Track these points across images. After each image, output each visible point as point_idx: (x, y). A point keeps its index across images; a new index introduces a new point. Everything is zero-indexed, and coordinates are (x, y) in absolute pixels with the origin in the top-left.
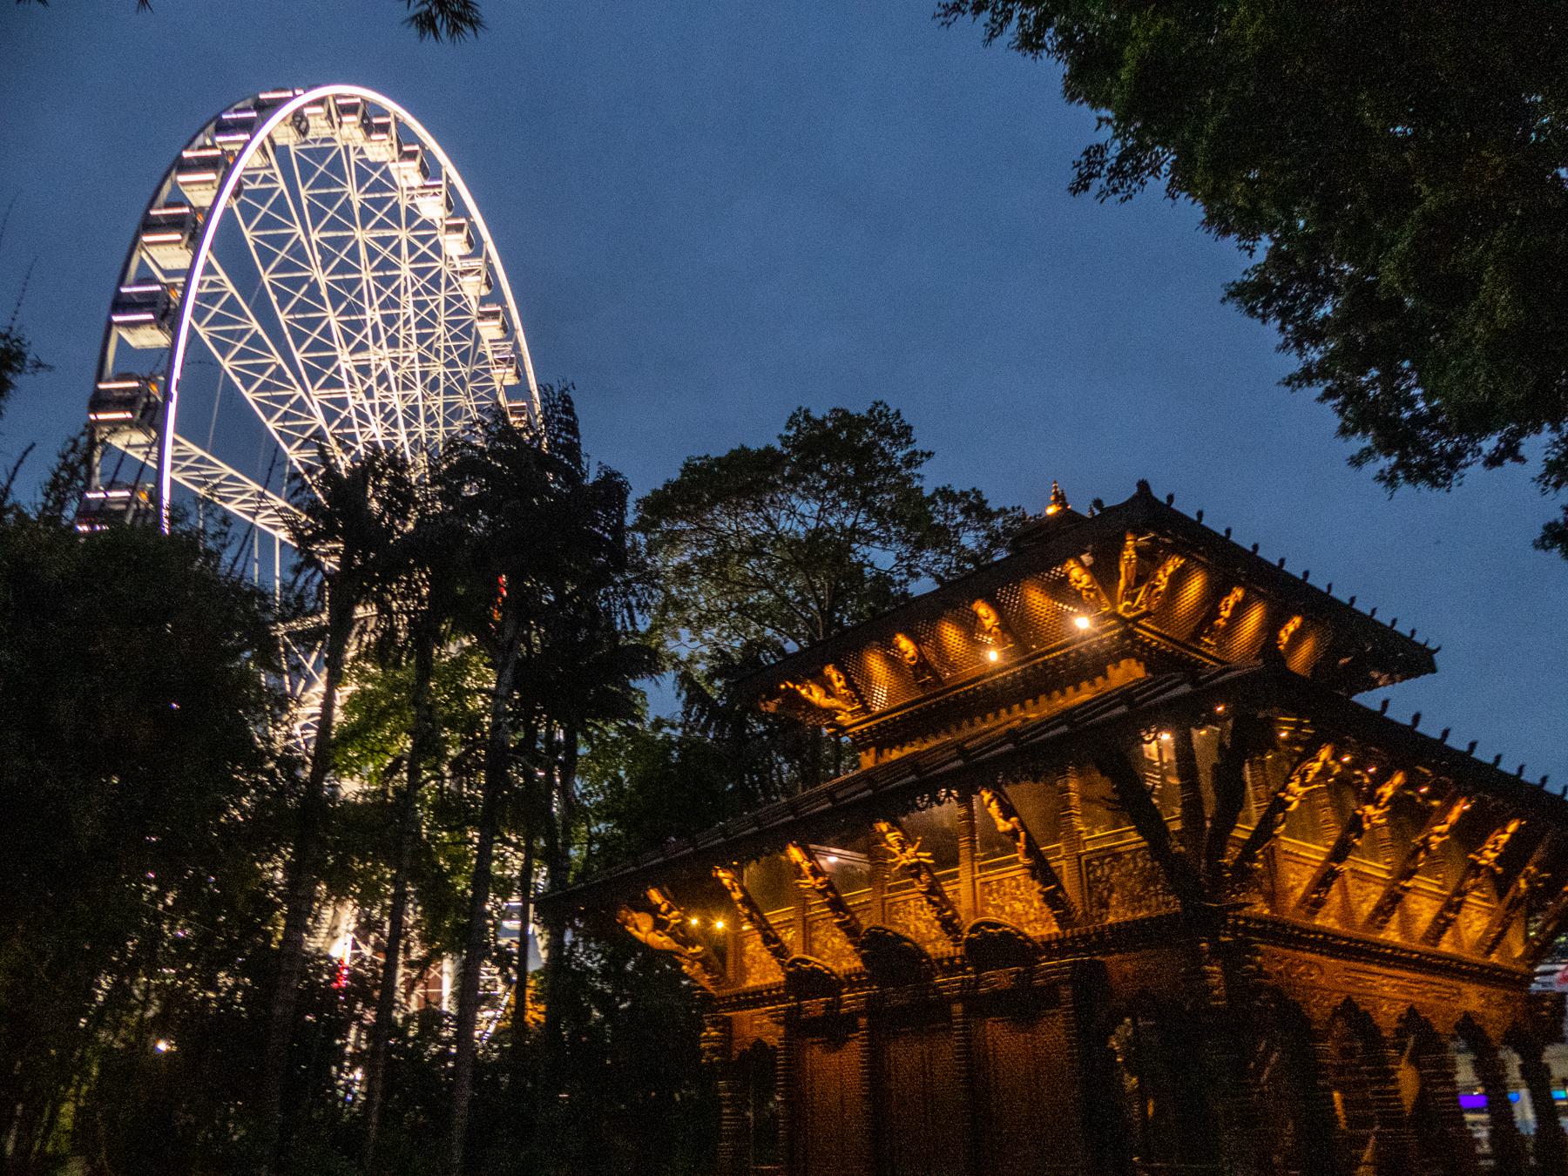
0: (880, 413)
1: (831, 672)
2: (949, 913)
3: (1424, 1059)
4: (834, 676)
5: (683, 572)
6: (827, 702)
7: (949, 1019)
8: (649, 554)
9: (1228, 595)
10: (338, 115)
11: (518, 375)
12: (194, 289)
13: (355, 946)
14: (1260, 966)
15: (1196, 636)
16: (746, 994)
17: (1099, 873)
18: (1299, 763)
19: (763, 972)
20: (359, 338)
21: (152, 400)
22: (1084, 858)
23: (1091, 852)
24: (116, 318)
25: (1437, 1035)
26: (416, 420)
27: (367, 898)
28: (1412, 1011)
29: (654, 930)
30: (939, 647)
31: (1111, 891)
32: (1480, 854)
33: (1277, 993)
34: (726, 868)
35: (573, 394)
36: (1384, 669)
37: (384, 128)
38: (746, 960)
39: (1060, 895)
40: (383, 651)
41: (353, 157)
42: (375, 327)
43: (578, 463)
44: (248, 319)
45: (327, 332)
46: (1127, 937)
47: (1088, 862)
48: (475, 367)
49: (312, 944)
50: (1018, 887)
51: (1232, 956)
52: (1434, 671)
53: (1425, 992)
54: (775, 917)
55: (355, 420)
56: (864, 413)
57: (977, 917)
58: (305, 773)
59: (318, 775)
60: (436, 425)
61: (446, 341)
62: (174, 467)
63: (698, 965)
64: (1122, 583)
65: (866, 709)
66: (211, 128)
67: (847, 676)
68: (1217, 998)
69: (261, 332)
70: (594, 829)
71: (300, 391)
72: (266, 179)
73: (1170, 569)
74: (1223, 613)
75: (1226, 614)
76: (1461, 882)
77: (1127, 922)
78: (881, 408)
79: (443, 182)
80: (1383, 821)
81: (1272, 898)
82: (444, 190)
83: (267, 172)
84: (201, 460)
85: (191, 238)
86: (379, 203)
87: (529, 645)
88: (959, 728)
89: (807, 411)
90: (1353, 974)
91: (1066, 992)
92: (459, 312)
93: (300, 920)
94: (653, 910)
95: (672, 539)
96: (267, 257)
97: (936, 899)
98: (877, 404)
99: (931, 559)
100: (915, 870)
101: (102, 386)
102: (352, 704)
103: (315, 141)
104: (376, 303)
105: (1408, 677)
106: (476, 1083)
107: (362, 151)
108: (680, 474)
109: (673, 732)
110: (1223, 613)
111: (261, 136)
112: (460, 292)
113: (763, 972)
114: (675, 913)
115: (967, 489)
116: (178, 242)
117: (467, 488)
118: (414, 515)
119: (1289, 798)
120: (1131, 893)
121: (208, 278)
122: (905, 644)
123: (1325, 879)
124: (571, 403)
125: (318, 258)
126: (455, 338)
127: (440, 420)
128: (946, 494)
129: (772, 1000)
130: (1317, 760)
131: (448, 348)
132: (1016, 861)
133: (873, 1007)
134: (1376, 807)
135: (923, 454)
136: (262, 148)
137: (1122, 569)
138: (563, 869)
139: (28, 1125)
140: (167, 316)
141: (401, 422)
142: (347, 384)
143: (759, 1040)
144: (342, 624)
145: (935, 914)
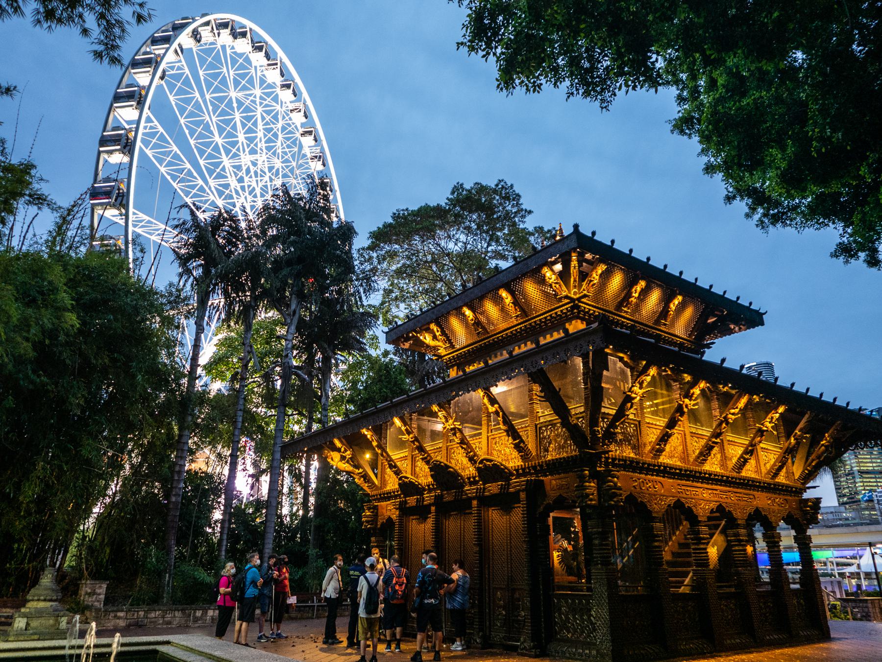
1: (433, 327)
3: (730, 532)
4: (435, 329)
6: (432, 343)
8: (379, 263)
9: (636, 285)
10: (217, 29)
11: (324, 165)
12: (141, 130)
14: (615, 484)
15: (619, 307)
16: (384, 494)
18: (638, 376)
19: (392, 484)
20: (234, 150)
21: (121, 191)
22: (538, 426)
23: (542, 423)
24: (101, 149)
25: (736, 519)
28: (720, 508)
29: (341, 461)
31: (550, 443)
32: (762, 424)
33: (631, 498)
36: (737, 323)
37: (244, 35)
38: (386, 476)
39: (522, 445)
41: (229, 51)
46: (555, 467)
47: (540, 428)
51: (601, 478)
52: (763, 324)
53: (731, 498)
55: (235, 196)
63: (362, 479)
65: (452, 346)
66: (149, 41)
68: (591, 500)
69: (178, 152)
71: (200, 182)
72: (179, 68)
73: (600, 272)
74: (634, 294)
75: (637, 295)
77: (556, 459)
78: (502, 183)
79: (279, 62)
81: (637, 447)
82: (279, 66)
83: (179, 64)
85: (138, 103)
86: (243, 76)
88: (496, 357)
89: (462, 185)
90: (683, 488)
91: (523, 495)
96: (182, 110)
97: (465, 446)
98: (500, 181)
103: (206, 44)
105: (749, 328)
107: (233, 48)
110: (634, 294)
111: (175, 45)
114: (348, 452)
115: (550, 228)
119: (633, 395)
120: (559, 445)
121: (149, 125)
122: (468, 312)
123: (664, 438)
125: (210, 108)
126: (288, 147)
128: (539, 230)
129: (396, 497)
130: (649, 375)
133: (438, 500)
134: (690, 400)
136: (176, 51)
140: (128, 147)
142: (229, 176)
143: (390, 517)
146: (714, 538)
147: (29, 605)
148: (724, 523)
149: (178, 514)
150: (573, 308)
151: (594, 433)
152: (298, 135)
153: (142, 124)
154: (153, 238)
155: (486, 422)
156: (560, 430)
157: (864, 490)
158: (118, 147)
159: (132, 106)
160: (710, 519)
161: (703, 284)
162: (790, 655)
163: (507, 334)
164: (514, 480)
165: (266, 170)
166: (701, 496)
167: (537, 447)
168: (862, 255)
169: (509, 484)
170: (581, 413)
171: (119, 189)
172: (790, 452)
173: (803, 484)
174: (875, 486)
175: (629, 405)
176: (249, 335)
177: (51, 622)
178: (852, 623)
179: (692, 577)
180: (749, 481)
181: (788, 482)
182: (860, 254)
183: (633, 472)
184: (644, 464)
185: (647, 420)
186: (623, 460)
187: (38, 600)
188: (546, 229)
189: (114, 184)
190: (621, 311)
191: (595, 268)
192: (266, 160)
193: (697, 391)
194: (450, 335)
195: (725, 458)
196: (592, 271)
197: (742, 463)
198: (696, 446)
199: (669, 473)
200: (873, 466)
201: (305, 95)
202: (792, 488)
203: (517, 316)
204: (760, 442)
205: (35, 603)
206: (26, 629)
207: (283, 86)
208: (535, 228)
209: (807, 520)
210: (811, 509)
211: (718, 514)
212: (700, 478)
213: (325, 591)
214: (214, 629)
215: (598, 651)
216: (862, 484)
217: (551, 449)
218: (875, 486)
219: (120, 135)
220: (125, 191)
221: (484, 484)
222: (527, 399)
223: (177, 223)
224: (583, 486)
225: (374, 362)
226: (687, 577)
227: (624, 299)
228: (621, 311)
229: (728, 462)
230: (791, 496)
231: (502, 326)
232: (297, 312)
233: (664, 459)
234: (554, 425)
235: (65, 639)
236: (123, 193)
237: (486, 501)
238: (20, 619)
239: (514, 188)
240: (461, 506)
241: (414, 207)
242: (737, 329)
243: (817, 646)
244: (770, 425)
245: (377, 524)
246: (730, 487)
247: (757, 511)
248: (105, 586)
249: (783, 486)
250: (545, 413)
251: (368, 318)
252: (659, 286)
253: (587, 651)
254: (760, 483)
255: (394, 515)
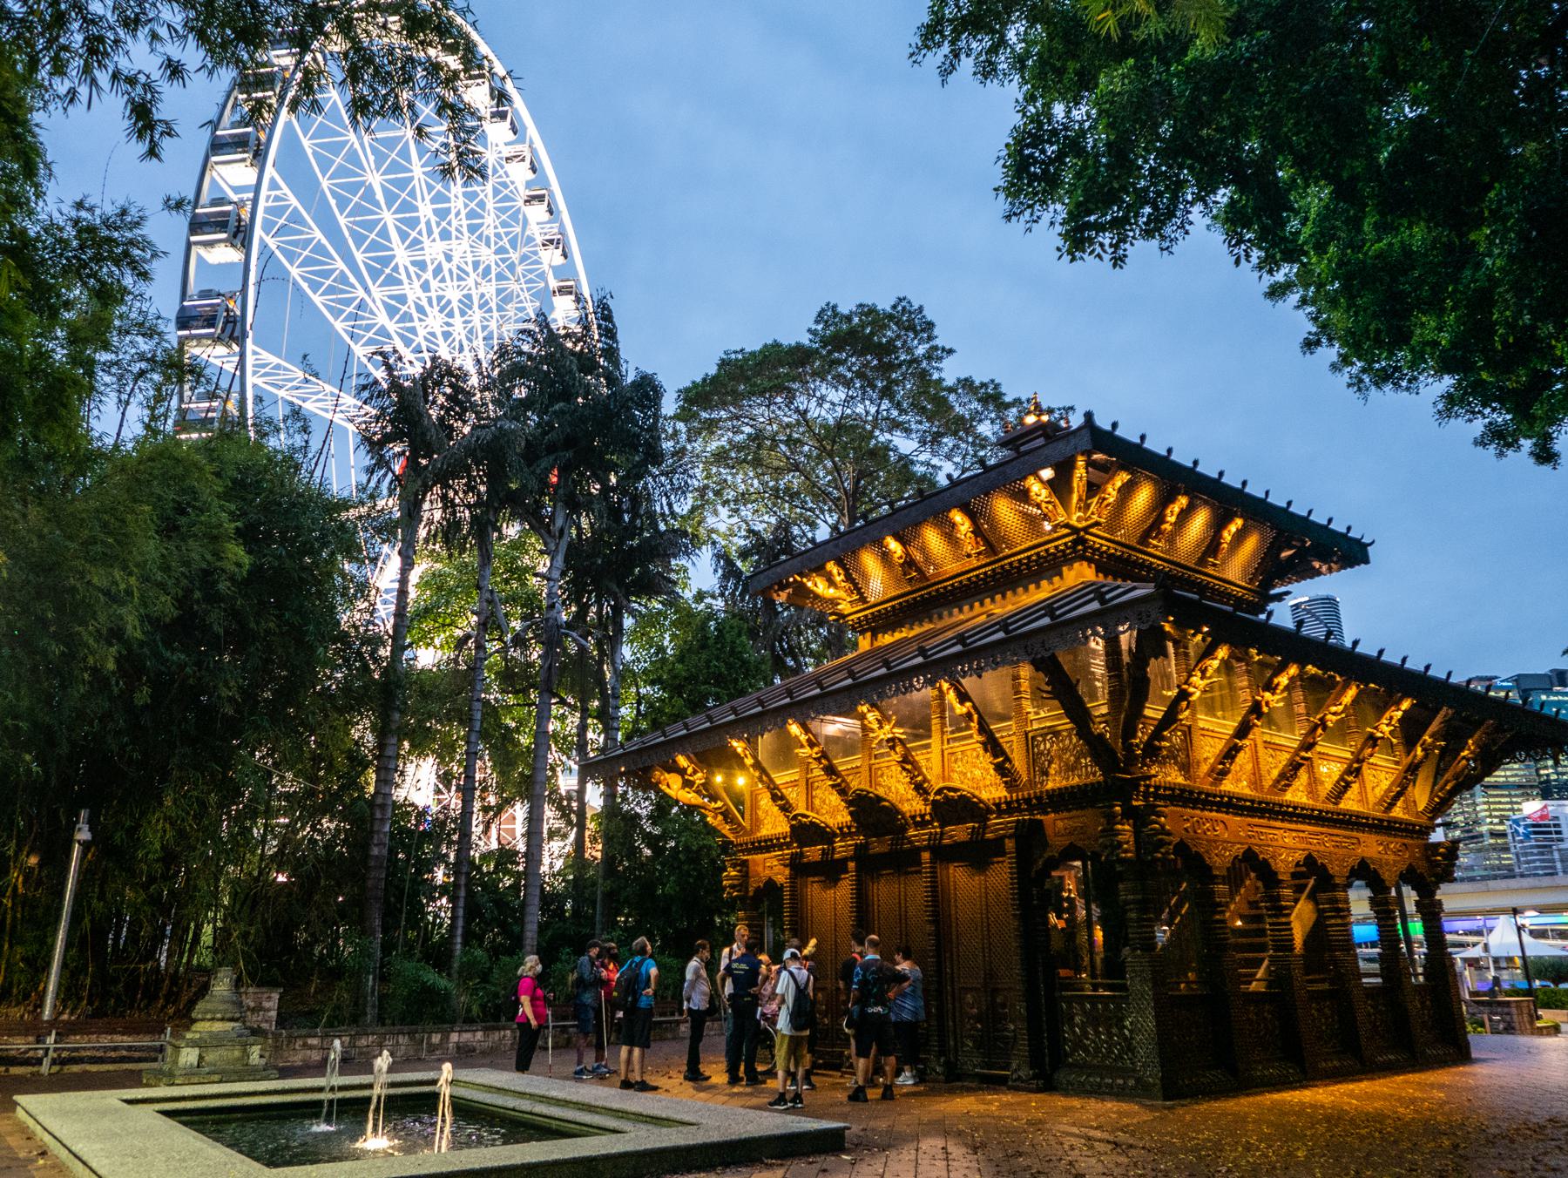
0: (904, 308)
1: (831, 567)
2: (920, 778)
3: (1323, 896)
4: (835, 571)
5: (720, 457)
7: (920, 864)
8: (689, 440)
11: (565, 255)
13: (438, 792)
14: (1163, 826)
15: (1144, 538)
16: (759, 842)
17: (1042, 747)
19: (774, 824)
20: (414, 234)
22: (1030, 735)
24: (193, 239)
26: (470, 308)
27: (445, 752)
28: (1310, 860)
29: (683, 787)
30: (923, 549)
31: (1050, 762)
32: (1376, 728)
33: (1182, 848)
34: (740, 739)
35: (610, 302)
36: (1324, 560)
38: (760, 813)
39: (1007, 765)
40: (449, 533)
42: (428, 223)
43: (617, 365)
44: (311, 228)
45: (384, 233)
46: (1061, 800)
48: (525, 250)
49: (399, 795)
50: (978, 756)
51: (1139, 818)
52: (1367, 561)
54: (780, 778)
55: (415, 315)
56: (889, 309)
57: (944, 781)
58: (385, 652)
59: (399, 649)
60: (490, 310)
61: (496, 227)
62: (255, 373)
63: (720, 817)
64: (1075, 497)
65: (863, 599)
67: (846, 571)
68: (1126, 851)
69: (324, 241)
70: (643, 691)
71: (361, 293)
73: (1119, 484)
74: (1169, 519)
75: (1173, 519)
76: (1362, 749)
80: (1281, 704)
81: (1186, 768)
84: (278, 367)
85: (256, 155)
87: (579, 528)
88: (941, 617)
89: (834, 307)
90: (1255, 829)
91: (1010, 844)
92: (506, 199)
93: (389, 773)
94: (682, 772)
95: (711, 426)
96: (325, 165)
97: (909, 767)
98: (900, 300)
99: (950, 445)
100: (892, 742)
101: (185, 303)
102: (424, 584)
104: (427, 198)
106: (544, 907)
108: (716, 367)
109: (714, 602)
112: (505, 179)
113: (774, 824)
114: (699, 775)
115: (986, 380)
116: (243, 160)
117: (517, 391)
118: (471, 417)
119: (1191, 690)
121: (273, 193)
122: (893, 545)
123: (1231, 753)
124: (610, 311)
125: (372, 158)
126: (504, 224)
127: (493, 305)
128: (967, 384)
129: (780, 847)
131: (498, 235)
132: (971, 736)
133: (860, 854)
134: (1273, 694)
135: (943, 349)
137: (1075, 485)
138: (613, 729)
139: (178, 939)
140: (240, 234)
141: (457, 312)
142: (406, 281)
143: (770, 879)
144: (412, 512)
145: (908, 780)
146: (1299, 906)
147: (198, 1026)
148: (1312, 882)
149: (383, 876)
150: (1075, 542)
151: (1129, 748)
152: (520, 203)
153: (264, 192)
154: (282, 393)
155: (938, 726)
156: (1067, 742)
157: (1490, 816)
158: (224, 236)
159: (243, 160)
160: (1294, 875)
161: (1277, 500)
162: (1419, 1083)
163: (961, 582)
164: (994, 820)
165: (470, 269)
166: (1281, 843)
167: (1028, 768)
168: (1527, 444)
169: (986, 827)
170: (1103, 715)
171: (227, 310)
172: (1413, 769)
173: (1432, 819)
174: (1509, 810)
175: (1184, 704)
176: (488, 572)
177: (237, 1053)
178: (1497, 1037)
179: (1268, 967)
180: (1351, 816)
181: (1406, 817)
182: (1522, 441)
183: (1184, 806)
184: (1200, 793)
185: (1201, 724)
186: (1170, 789)
187: (213, 1019)
188: (977, 383)
189: (218, 301)
190: (1148, 545)
191: (1112, 478)
192: (469, 249)
193: (1283, 680)
194: (859, 581)
195: (1314, 781)
196: (1107, 482)
197: (1342, 788)
198: (1273, 766)
199: (1236, 807)
200: (1505, 776)
201: (532, 131)
202: (1414, 825)
203: (979, 553)
204: (1371, 755)
205: (208, 1024)
206: (198, 1066)
207: (493, 115)
208: (959, 381)
209: (1436, 875)
210: (1445, 859)
211: (1304, 869)
212: (1279, 813)
213: (688, 1000)
214: (514, 1061)
215: (1138, 1080)
216: (1486, 807)
217: (1052, 771)
218: (1509, 810)
219: (227, 214)
220: (238, 313)
221: (942, 827)
222: (1009, 689)
223: (365, 382)
224: (1113, 830)
225: (686, 618)
226: (1259, 968)
227: (1153, 525)
228: (1148, 545)
229: (1319, 788)
230: (1412, 838)
231: (952, 567)
232: (566, 531)
233: (1228, 786)
234: (1056, 734)
235: (324, 1076)
236: (235, 316)
237: (944, 853)
238: (189, 1049)
239: (924, 313)
240: (902, 861)
241: (754, 345)
242: (1324, 568)
243: (1454, 1070)
244: (1387, 729)
245: (747, 892)
246: (1323, 826)
247: (1363, 863)
248: (276, 996)
249: (1401, 823)
250: (1045, 716)
251: (682, 540)
252: (1206, 503)
253: (1120, 1081)
254: (1367, 818)
255: (781, 875)
